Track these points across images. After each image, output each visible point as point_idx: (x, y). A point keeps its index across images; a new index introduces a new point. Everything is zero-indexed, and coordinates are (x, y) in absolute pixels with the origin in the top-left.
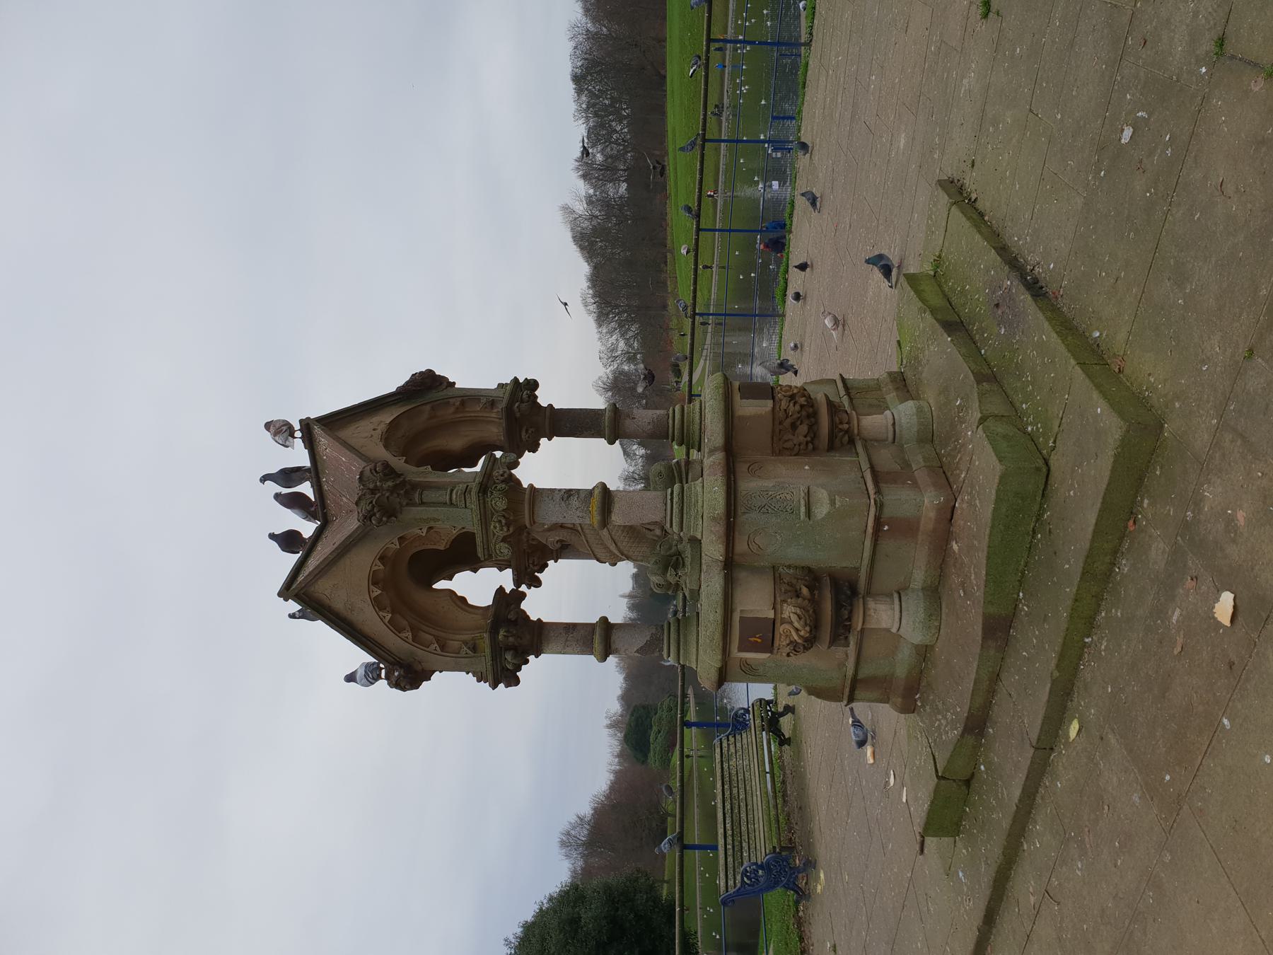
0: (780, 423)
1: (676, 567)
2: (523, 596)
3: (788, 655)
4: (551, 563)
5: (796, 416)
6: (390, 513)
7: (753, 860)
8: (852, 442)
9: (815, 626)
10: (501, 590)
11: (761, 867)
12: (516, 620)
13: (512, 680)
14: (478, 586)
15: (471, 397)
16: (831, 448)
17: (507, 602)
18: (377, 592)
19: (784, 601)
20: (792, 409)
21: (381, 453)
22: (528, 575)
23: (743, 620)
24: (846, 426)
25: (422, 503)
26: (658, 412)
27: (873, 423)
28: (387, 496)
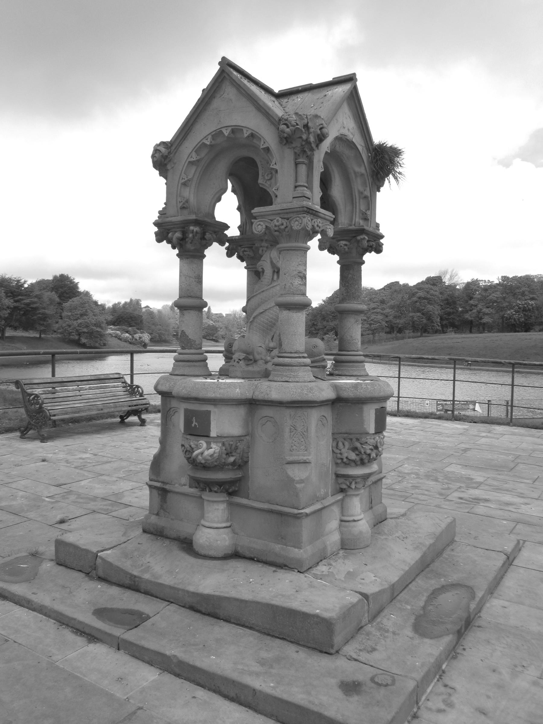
0: (358, 440)
1: (246, 359)
2: (222, 244)
3: (183, 445)
4: (244, 264)
5: (363, 451)
6: (286, 140)
7: (46, 401)
8: (342, 490)
9: (205, 467)
10: (226, 227)
11: (41, 407)
12: (205, 239)
13: (160, 237)
14: (228, 211)
15: (370, 203)
16: (338, 476)
17: (215, 232)
18: (226, 132)
19: (223, 444)
20: (368, 448)
21: (333, 133)
22: (235, 248)
24: (353, 486)
25: (296, 164)
26: (360, 343)
27: (356, 506)
28: (300, 138)
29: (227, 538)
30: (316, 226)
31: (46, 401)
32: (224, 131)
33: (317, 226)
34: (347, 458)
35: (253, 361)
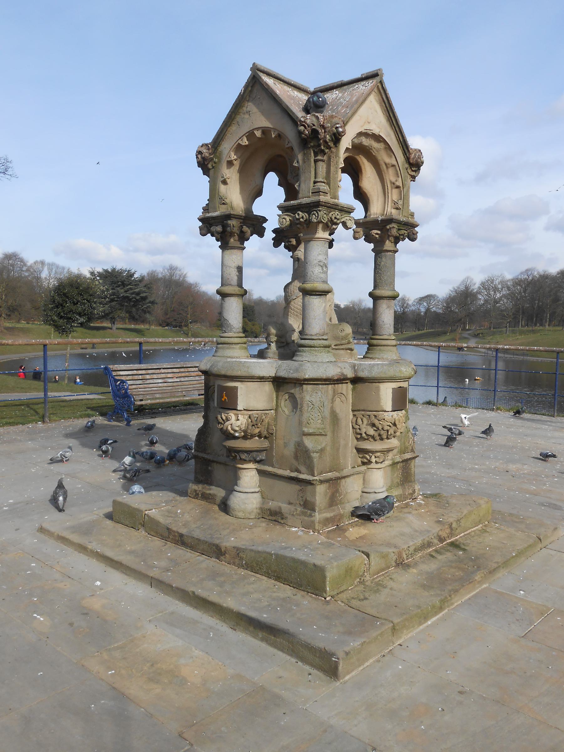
5: (380, 428)
11: (126, 392)
17: (256, 225)
22: (281, 237)
23: (236, 388)
24: (373, 460)
25: (316, 161)
29: (255, 502)
30: (333, 218)
31: (130, 387)
32: (256, 132)
33: (335, 218)
34: (365, 433)
35: (285, 344)
